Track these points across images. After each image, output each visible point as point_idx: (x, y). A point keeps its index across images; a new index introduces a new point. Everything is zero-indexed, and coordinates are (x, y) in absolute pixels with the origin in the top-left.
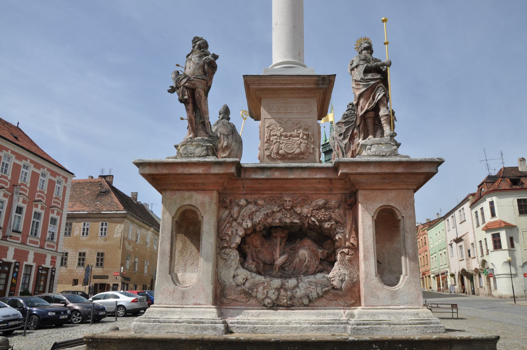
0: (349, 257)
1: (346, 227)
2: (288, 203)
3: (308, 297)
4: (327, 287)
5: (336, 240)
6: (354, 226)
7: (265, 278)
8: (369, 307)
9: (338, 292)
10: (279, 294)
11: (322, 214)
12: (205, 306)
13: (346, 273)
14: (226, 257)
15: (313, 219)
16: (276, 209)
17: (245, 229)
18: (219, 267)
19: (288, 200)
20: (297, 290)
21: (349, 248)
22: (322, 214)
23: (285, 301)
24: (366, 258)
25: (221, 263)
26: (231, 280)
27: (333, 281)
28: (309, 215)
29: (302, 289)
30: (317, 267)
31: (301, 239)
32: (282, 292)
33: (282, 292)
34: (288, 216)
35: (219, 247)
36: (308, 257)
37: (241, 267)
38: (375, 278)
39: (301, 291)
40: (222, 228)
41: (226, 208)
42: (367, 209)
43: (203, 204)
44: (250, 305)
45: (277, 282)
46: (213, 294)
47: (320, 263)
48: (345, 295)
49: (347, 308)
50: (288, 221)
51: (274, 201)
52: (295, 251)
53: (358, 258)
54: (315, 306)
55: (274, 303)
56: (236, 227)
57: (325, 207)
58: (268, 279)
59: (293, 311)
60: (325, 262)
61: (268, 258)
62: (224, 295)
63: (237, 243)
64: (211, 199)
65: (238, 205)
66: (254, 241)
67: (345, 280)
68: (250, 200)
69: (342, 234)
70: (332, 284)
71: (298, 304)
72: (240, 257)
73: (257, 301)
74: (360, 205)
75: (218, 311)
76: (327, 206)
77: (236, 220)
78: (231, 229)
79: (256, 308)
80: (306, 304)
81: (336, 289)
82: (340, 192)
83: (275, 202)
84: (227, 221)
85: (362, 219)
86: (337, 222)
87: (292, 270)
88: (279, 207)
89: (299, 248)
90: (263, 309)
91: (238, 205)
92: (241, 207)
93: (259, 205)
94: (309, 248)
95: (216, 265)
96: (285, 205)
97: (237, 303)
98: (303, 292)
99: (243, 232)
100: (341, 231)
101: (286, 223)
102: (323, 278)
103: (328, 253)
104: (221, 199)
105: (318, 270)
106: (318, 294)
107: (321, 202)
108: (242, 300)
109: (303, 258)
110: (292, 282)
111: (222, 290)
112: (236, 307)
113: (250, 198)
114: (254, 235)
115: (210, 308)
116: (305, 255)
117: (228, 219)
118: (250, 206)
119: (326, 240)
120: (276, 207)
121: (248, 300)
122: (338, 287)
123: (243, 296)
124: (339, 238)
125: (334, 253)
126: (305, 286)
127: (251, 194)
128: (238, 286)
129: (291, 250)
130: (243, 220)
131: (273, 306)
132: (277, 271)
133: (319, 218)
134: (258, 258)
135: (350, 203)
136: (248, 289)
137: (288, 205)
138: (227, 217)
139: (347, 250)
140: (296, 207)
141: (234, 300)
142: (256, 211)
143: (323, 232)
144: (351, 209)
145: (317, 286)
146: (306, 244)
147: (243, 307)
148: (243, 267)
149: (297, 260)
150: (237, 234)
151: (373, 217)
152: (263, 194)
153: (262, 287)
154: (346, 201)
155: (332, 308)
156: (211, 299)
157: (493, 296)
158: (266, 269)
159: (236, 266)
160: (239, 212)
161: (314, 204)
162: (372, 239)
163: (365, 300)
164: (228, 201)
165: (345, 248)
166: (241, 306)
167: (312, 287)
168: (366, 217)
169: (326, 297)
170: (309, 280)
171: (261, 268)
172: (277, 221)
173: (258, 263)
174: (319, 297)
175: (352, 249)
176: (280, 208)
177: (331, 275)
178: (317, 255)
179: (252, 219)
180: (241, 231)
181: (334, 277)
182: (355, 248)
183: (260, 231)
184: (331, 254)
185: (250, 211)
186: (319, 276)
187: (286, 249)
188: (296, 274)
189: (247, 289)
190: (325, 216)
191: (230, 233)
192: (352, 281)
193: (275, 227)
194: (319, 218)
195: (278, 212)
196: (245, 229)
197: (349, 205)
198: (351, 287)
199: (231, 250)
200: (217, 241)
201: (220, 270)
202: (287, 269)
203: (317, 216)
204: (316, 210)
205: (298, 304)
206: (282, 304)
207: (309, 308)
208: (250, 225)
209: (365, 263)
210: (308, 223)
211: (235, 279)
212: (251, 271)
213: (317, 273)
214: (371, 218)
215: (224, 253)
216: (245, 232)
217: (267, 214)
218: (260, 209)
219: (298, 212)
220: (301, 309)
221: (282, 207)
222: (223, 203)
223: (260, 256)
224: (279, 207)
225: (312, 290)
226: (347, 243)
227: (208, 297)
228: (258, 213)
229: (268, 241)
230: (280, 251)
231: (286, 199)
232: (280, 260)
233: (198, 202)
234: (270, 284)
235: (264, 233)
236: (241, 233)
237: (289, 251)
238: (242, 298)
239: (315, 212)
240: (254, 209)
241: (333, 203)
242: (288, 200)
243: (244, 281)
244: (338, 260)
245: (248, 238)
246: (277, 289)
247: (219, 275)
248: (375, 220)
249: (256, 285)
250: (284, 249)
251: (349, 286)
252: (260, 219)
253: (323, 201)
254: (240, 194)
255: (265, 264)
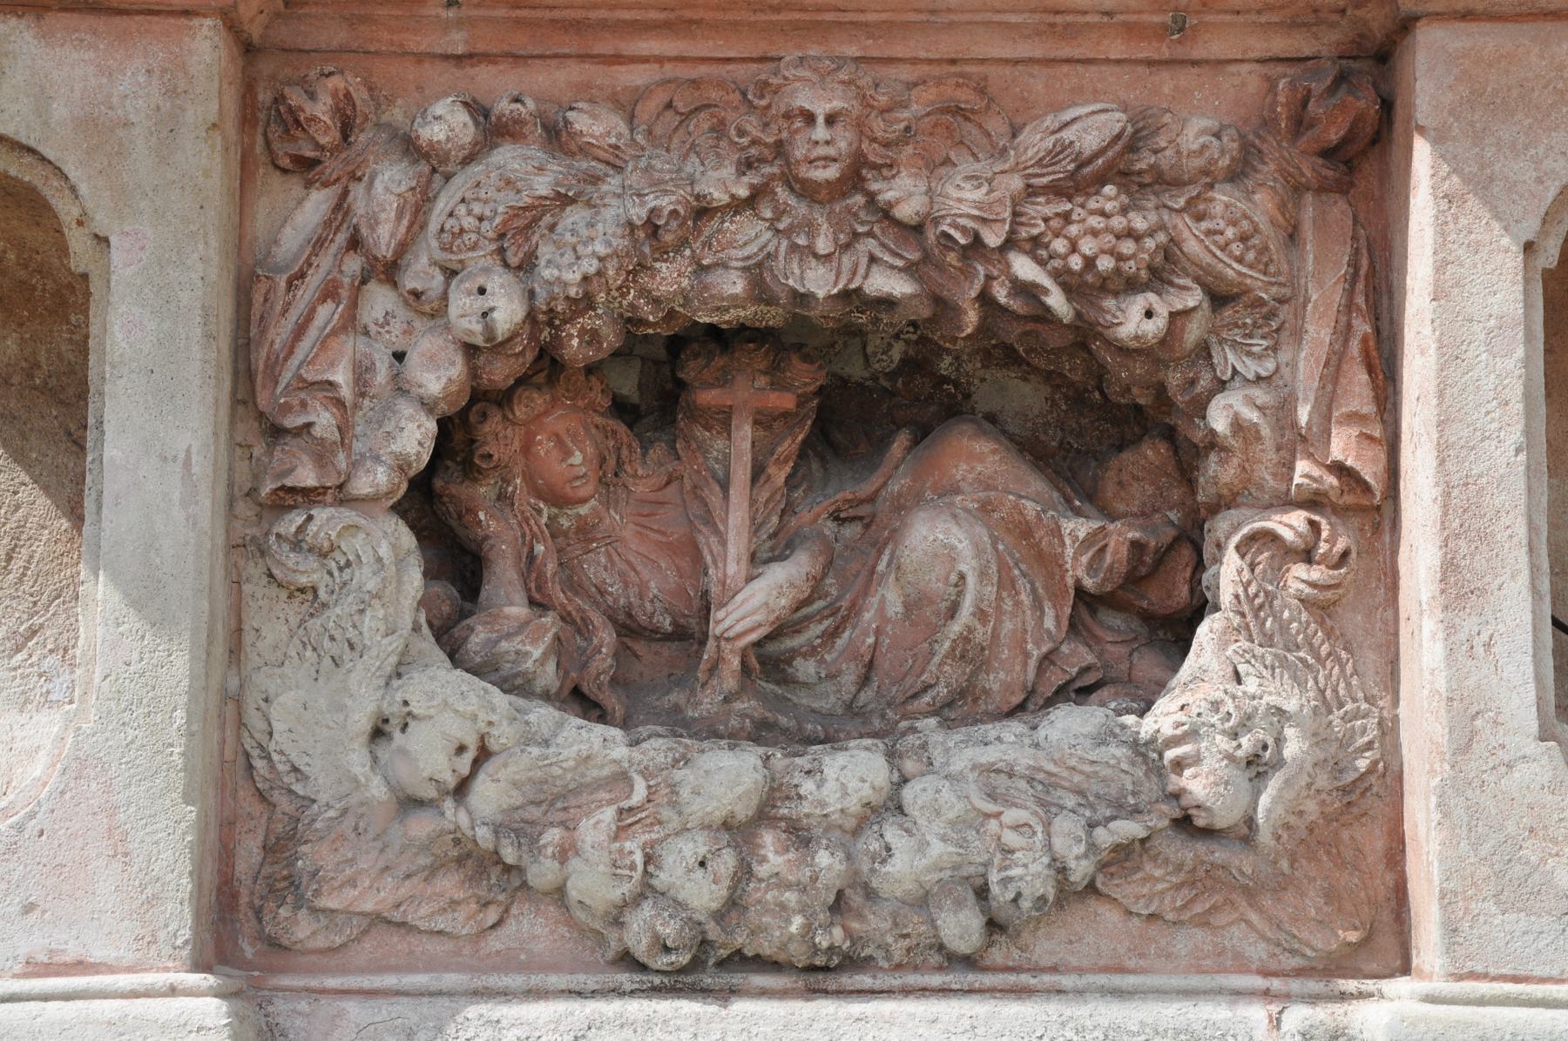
0: (1316, 573)
1: (1298, 335)
2: (820, 132)
3: (982, 893)
4: (1136, 811)
5: (1213, 443)
6: (1362, 327)
7: (634, 743)
8: (1484, 988)
9: (1219, 854)
10: (745, 872)
11: (1096, 230)
12: (124, 981)
13: (1291, 705)
14: (307, 571)
15: (1024, 268)
16: (721, 182)
17: (470, 350)
18: (252, 658)
19: (821, 109)
20: (892, 834)
21: (1313, 501)
22: (1096, 230)
23: (797, 923)
24: (1458, 587)
25: (272, 624)
26: (357, 760)
27: (1179, 765)
28: (993, 239)
29: (932, 830)
30: (1047, 659)
31: (922, 433)
32: (773, 855)
33: (773, 855)
34: (823, 245)
35: (252, 493)
36: (983, 574)
37: (440, 656)
38: (1533, 747)
39: (923, 846)
40: (280, 333)
41: (305, 168)
42: (1477, 182)
43: (99, 129)
44: (507, 963)
45: (728, 776)
46: (197, 874)
47: (1074, 627)
48: (1282, 885)
49: (1295, 985)
50: (820, 282)
51: (704, 121)
52: (871, 527)
53: (1394, 587)
54: (1037, 970)
55: (705, 943)
56: (395, 336)
57: (1126, 168)
58: (657, 749)
59: (857, 1008)
60: (1115, 620)
61: (654, 586)
62: (293, 882)
63: (402, 465)
64: (171, 92)
65: (411, 148)
66: (544, 446)
67: (1279, 763)
68: (504, 107)
69: (1261, 395)
70: (1176, 796)
71: (898, 956)
72: (428, 575)
73: (571, 923)
74: (1422, 153)
75: (238, 1017)
76: (1144, 161)
77: (390, 271)
78: (349, 346)
79: (555, 981)
80: (962, 947)
81: (1209, 833)
82: (1259, 46)
83: (719, 129)
84: (314, 281)
85: (1440, 267)
86: (1219, 298)
87: (849, 678)
88: (747, 165)
89: (903, 507)
90: (618, 992)
91: (411, 148)
92: (434, 164)
93: (585, 151)
94: (986, 508)
95: (232, 644)
96: (799, 153)
97: (398, 943)
98: (937, 848)
99: (456, 369)
100: (1250, 368)
101: (802, 298)
102: (1100, 741)
103: (1136, 546)
104: (264, 96)
105: (1056, 678)
106: (1060, 870)
107: (1092, 129)
108: (441, 923)
109: (935, 583)
110: (848, 774)
111: (280, 847)
112: (389, 981)
113: (503, 88)
114: (540, 400)
115: (173, 991)
116: (952, 558)
117: (325, 262)
118: (507, 156)
119: (1120, 448)
120: (728, 172)
121: (492, 915)
122: (1225, 814)
123: (449, 884)
124: (1238, 425)
125: (1191, 544)
126: (954, 805)
127: (517, 59)
128: (410, 803)
129: (836, 518)
130: (450, 273)
131: (696, 964)
132: (730, 683)
133: (1076, 263)
134: (574, 585)
135: (1334, 136)
136: (497, 830)
137: (822, 151)
138: (319, 244)
139: (1298, 518)
140: (888, 168)
141: (378, 920)
142: (563, 200)
143: (1100, 375)
144: (1342, 188)
145: (1048, 809)
146: (960, 471)
147: (450, 979)
148: (455, 655)
149: (890, 597)
150: (400, 387)
151: (1529, 247)
152: (617, 59)
153: (608, 814)
154: (1300, 123)
155: (1176, 981)
156: (178, 918)
157: (334, 333)
158: (639, 666)
159: (395, 643)
160: (419, 207)
161: (1035, 142)
162: (1515, 435)
163: (1451, 930)
164: (321, 109)
165: (1287, 502)
166: (430, 966)
167: (1012, 815)
168: (1476, 248)
169: (1126, 890)
170: (990, 755)
171: (603, 661)
172: (734, 284)
173: (576, 624)
174: (1070, 894)
175: (1340, 512)
176: (753, 178)
177: (1163, 718)
178: (1048, 562)
179: (527, 266)
180: (432, 361)
181: (1192, 734)
182: (1370, 506)
183: (591, 370)
184: (1164, 555)
185: (510, 199)
186: (1070, 725)
187: (805, 515)
188: (880, 708)
189: (483, 835)
190: (1128, 247)
191: (341, 376)
192: (1338, 769)
193: (713, 331)
194: (1076, 263)
195: (737, 206)
196: (470, 350)
197: (1328, 153)
198: (1328, 819)
199: (348, 515)
200: (238, 446)
201: (264, 681)
202: (806, 669)
203: (1060, 245)
204: (1057, 191)
205: (898, 949)
206: (767, 949)
207: (988, 980)
208: (507, 311)
209: (1450, 629)
210: (985, 298)
211: (384, 752)
212: (518, 686)
213: (1050, 702)
214: (1513, 261)
215: (296, 544)
216: (473, 373)
217: (652, 228)
218: (595, 180)
219: (906, 212)
220: (924, 992)
221: (774, 172)
222: (275, 136)
223: (595, 568)
224: (747, 165)
225: (1010, 838)
226: (1302, 466)
227: (151, 902)
228: (574, 216)
229: (657, 452)
230: (756, 527)
231: (804, 99)
232: (752, 602)
233: (59, 111)
234: (673, 788)
235: (627, 384)
236: (438, 375)
237: (829, 528)
238: (444, 903)
239: (1042, 208)
240: (542, 186)
241: (1194, 134)
242: (821, 109)
243: (464, 764)
244: (1226, 598)
245: (494, 424)
246: (726, 825)
247: (255, 720)
248: (1548, 276)
249: (557, 800)
250: (788, 510)
251: (1311, 807)
252: (590, 266)
253: (1115, 121)
254: (420, 58)
255: (629, 629)
